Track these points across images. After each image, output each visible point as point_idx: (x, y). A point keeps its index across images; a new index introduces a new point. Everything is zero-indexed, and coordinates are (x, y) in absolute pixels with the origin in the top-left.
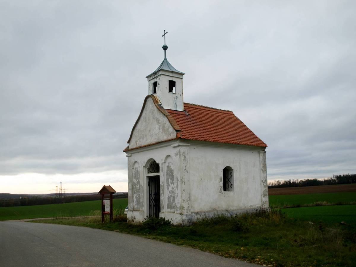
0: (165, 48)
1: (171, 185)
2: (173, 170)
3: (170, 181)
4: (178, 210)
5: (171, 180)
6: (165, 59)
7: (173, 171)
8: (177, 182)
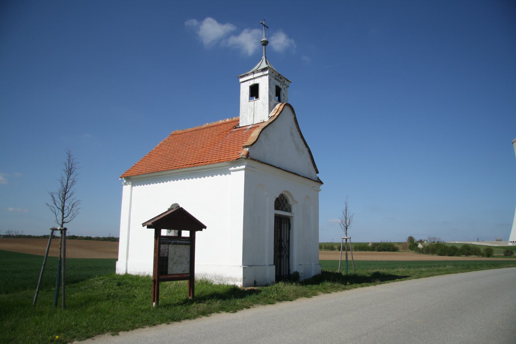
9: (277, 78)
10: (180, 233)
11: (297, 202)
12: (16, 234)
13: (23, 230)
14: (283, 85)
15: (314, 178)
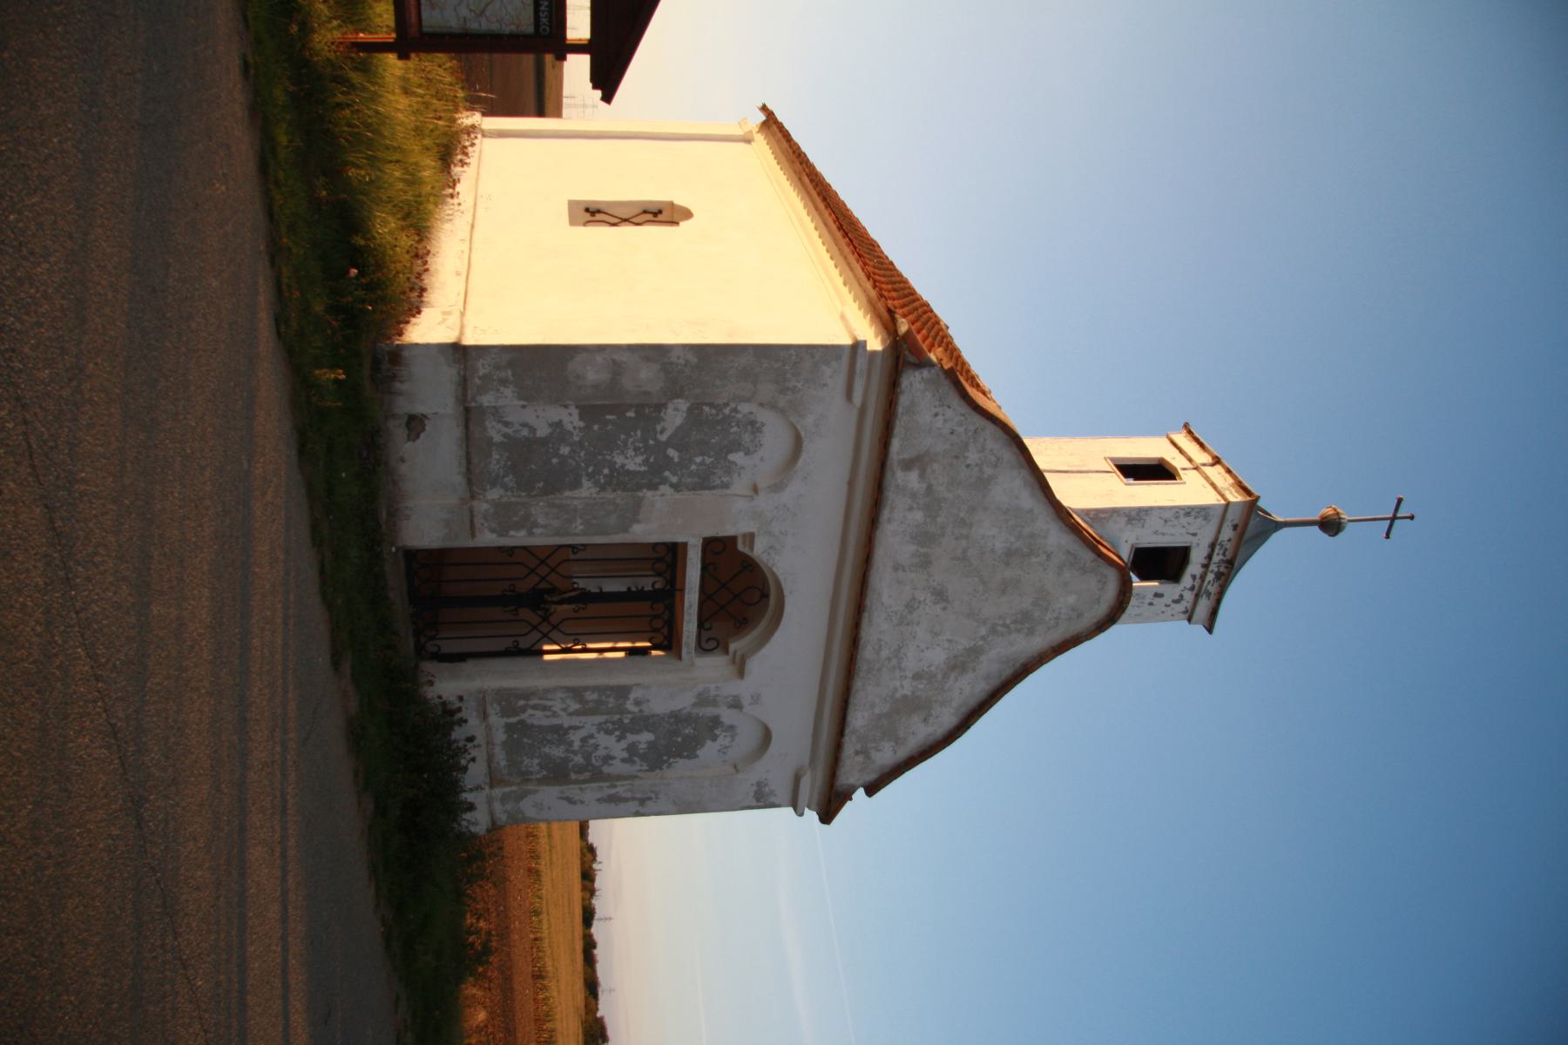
0: (1331, 525)
1: (624, 744)
2: (696, 756)
3: (646, 737)
4: (508, 807)
5: (649, 743)
6: (1279, 526)
7: (688, 757)
8: (634, 799)
9: (1216, 551)
10: (578, 48)
11: (741, 673)
12: (922, 373)
13: (610, 919)
14: (1192, 588)
15: (846, 776)
